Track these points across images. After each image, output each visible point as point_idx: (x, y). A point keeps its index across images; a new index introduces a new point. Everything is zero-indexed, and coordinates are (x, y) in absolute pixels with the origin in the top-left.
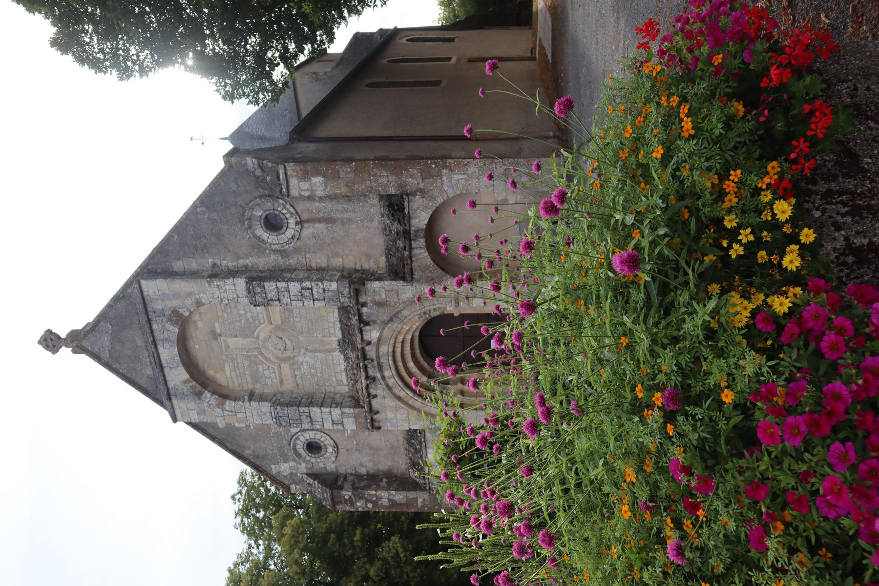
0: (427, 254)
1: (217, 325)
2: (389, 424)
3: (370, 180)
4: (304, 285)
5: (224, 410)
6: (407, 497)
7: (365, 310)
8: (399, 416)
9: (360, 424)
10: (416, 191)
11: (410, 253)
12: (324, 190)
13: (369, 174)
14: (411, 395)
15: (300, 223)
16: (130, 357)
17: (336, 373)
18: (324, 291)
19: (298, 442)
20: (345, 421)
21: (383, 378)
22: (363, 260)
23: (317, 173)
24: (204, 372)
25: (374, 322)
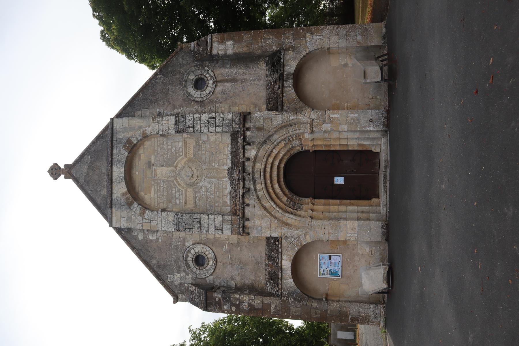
0: (293, 91)
2: (255, 231)
3: (261, 42)
4: (211, 115)
5: (144, 218)
6: (263, 302)
7: (248, 133)
8: (264, 224)
9: (234, 230)
10: (289, 48)
11: (283, 90)
12: (233, 49)
13: (261, 38)
14: (274, 206)
15: (216, 82)
16: (96, 181)
18: (223, 119)
19: (190, 255)
20: (224, 226)
21: (255, 190)
22: (252, 108)
23: (229, 39)
24: (138, 193)
25: (254, 143)
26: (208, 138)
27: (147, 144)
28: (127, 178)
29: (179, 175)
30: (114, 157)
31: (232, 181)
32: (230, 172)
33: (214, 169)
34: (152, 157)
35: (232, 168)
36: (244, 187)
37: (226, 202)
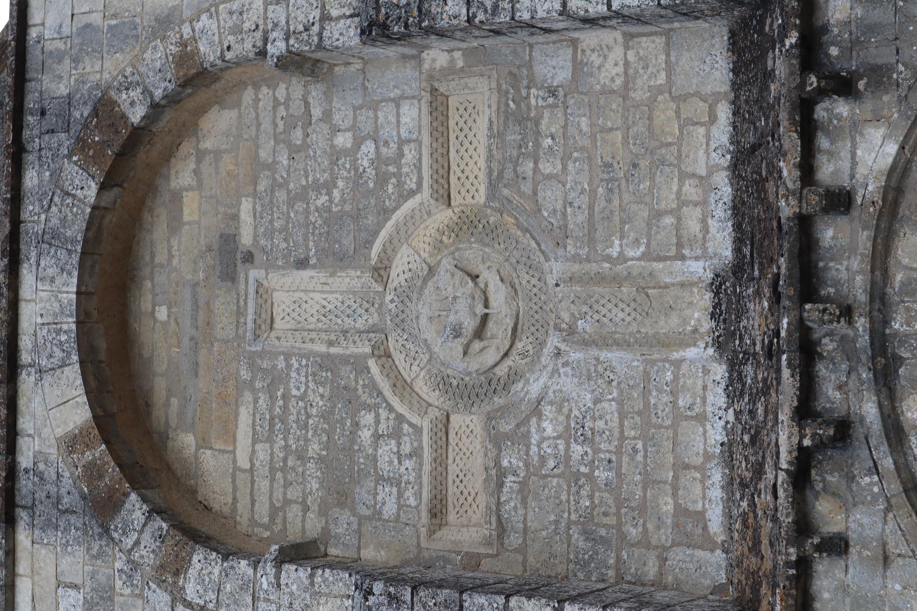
25: (879, 76)
26: (578, 66)
27: (218, 125)
28: (102, 344)
29: (400, 324)
30: (30, 209)
31: (735, 367)
32: (728, 293)
33: (617, 280)
34: (246, 205)
35: (739, 268)
36: (805, 411)
37: (700, 517)
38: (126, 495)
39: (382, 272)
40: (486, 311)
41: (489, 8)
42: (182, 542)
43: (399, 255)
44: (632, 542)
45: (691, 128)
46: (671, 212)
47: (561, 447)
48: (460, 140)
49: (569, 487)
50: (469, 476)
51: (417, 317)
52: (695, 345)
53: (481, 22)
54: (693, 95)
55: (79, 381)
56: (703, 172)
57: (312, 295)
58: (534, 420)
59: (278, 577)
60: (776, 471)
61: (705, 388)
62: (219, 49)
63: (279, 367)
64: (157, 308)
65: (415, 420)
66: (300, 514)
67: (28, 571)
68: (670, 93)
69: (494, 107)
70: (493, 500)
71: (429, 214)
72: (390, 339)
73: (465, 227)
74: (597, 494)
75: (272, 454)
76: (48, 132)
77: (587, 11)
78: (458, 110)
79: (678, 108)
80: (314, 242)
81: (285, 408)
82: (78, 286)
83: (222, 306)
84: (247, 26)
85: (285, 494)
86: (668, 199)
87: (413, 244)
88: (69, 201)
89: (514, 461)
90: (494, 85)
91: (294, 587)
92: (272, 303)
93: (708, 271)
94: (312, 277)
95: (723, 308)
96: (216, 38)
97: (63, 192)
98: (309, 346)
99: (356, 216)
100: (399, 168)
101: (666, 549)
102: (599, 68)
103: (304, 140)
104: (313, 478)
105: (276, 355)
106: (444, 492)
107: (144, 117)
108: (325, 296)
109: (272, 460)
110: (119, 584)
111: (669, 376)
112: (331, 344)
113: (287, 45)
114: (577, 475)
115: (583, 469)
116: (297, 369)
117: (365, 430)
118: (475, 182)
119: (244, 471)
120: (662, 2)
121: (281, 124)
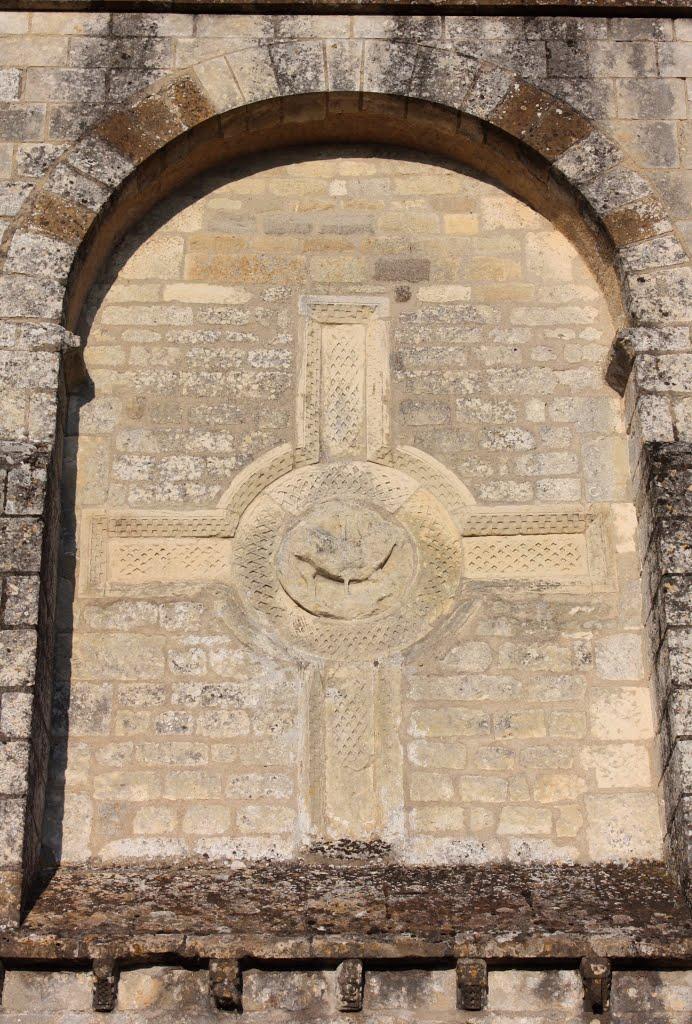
1: (460, 292)
17: (181, 809)
29: (330, 480)
32: (367, 862)
35: (397, 875)
37: (126, 832)
38: (131, 158)
39: (388, 458)
40: (347, 582)
41: (682, 599)
42: (79, 229)
43: (406, 477)
44: (97, 754)
45: (549, 817)
46: (457, 794)
47: (198, 672)
48: (536, 548)
49: (156, 681)
50: (163, 563)
51: (337, 500)
52: (313, 823)
53: (665, 590)
54: (585, 819)
55: (259, 96)
56: (500, 832)
57: (361, 372)
58: (228, 641)
59: (45, 348)
60: (184, 932)
61: (268, 835)
62: (640, 268)
63: (280, 336)
64: (344, 182)
65: (225, 500)
66: (114, 363)
67: (36, 30)
68: (588, 793)
69: (572, 589)
70: (135, 593)
71: (453, 513)
72: (314, 467)
73: (439, 556)
74: (148, 714)
75: (182, 328)
76: (548, 50)
77: (676, 712)
78: (570, 545)
79: (571, 803)
80: (422, 377)
81: (234, 343)
82: (369, 93)
83: (351, 265)
84: (665, 300)
85: (136, 344)
86: (472, 791)
87: (419, 494)
88: (468, 81)
89: (181, 617)
90: (597, 589)
91: (33, 368)
92: (351, 324)
93: (394, 837)
94: (381, 375)
95: (355, 855)
96: (653, 264)
97: (477, 61)
98: (304, 371)
99: (451, 428)
100: (504, 479)
101: (90, 793)
102: (615, 711)
103: (536, 362)
104: (156, 379)
105: (293, 331)
106: (145, 534)
107: (564, 175)
108: (360, 388)
109: (176, 328)
110: (28, 147)
111: (278, 794)
112: (307, 397)
113: (644, 353)
114: (166, 689)
115: (175, 697)
116: (278, 358)
117: (211, 441)
118: (489, 566)
119: (160, 294)
120: (686, 799)
121: (554, 334)
